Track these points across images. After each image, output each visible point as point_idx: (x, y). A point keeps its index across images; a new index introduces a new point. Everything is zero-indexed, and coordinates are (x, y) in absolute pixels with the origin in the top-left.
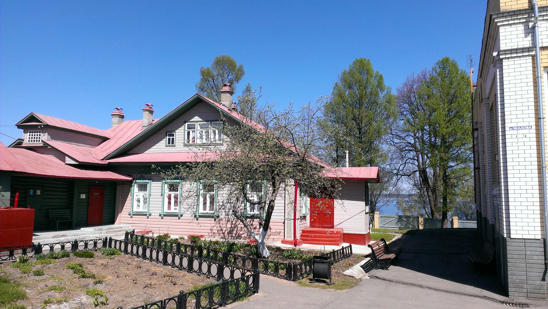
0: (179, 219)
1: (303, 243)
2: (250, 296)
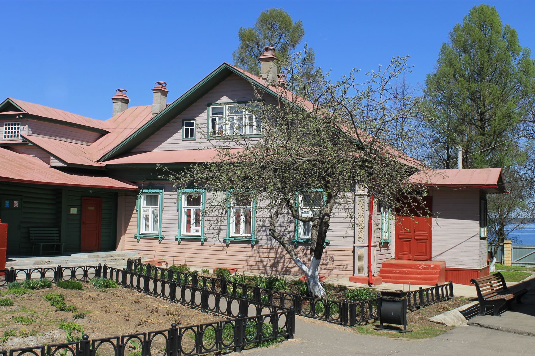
0: (202, 244)
1: (383, 281)
2: (280, 342)
